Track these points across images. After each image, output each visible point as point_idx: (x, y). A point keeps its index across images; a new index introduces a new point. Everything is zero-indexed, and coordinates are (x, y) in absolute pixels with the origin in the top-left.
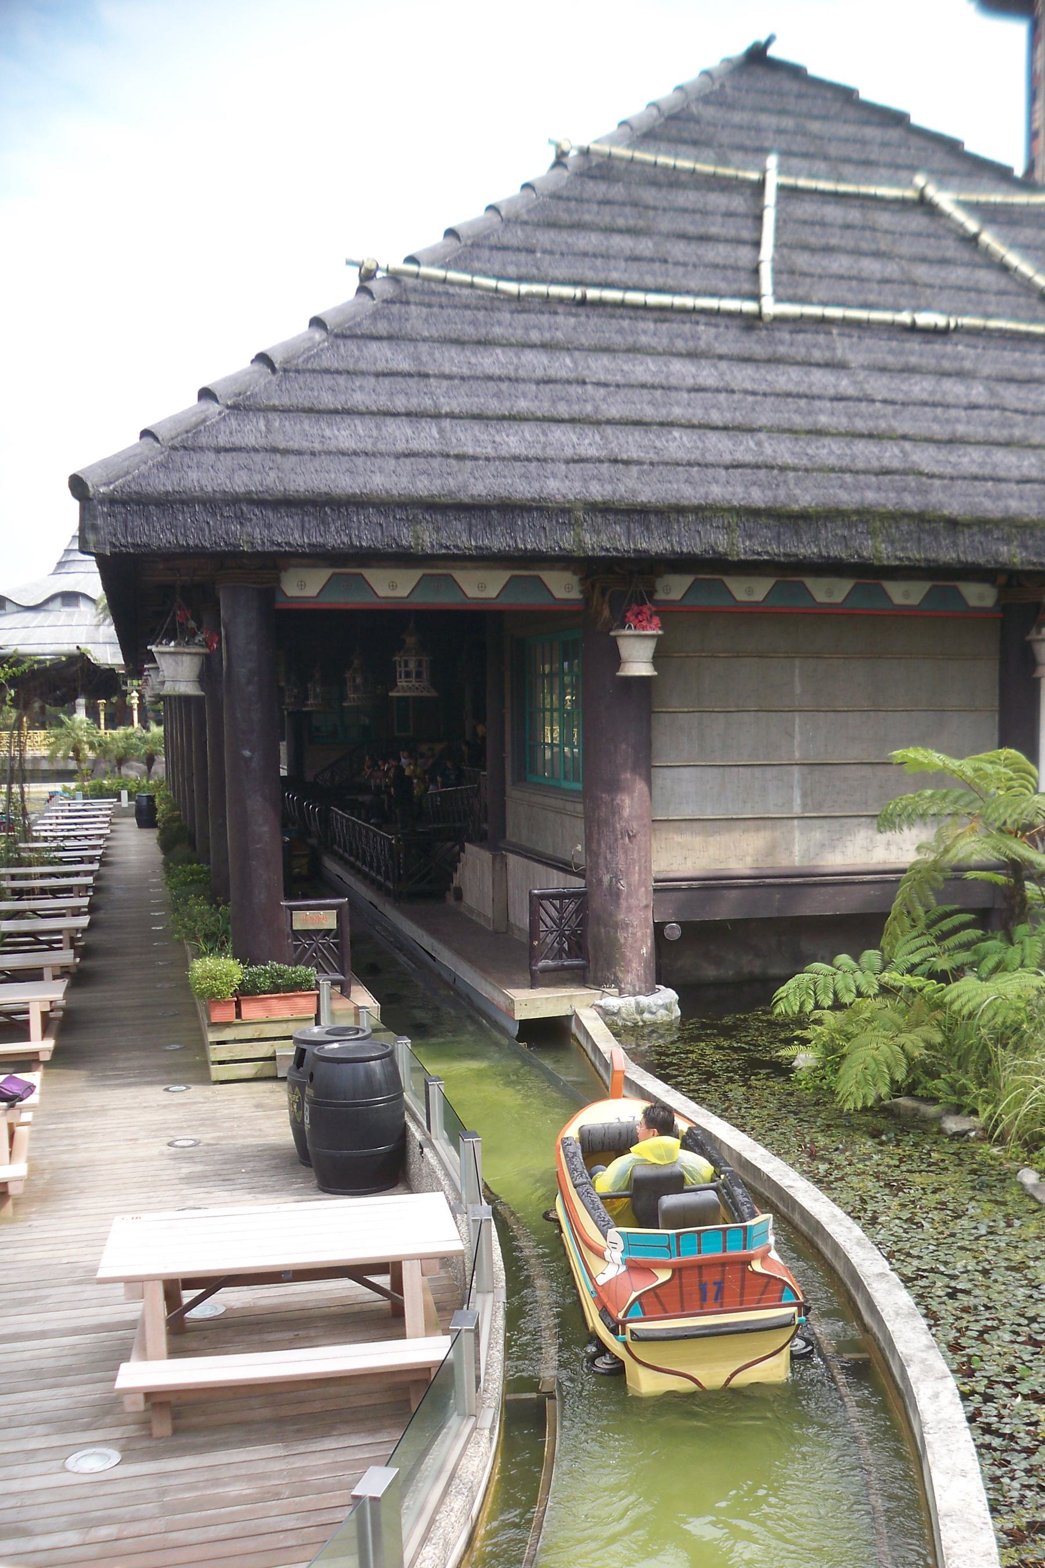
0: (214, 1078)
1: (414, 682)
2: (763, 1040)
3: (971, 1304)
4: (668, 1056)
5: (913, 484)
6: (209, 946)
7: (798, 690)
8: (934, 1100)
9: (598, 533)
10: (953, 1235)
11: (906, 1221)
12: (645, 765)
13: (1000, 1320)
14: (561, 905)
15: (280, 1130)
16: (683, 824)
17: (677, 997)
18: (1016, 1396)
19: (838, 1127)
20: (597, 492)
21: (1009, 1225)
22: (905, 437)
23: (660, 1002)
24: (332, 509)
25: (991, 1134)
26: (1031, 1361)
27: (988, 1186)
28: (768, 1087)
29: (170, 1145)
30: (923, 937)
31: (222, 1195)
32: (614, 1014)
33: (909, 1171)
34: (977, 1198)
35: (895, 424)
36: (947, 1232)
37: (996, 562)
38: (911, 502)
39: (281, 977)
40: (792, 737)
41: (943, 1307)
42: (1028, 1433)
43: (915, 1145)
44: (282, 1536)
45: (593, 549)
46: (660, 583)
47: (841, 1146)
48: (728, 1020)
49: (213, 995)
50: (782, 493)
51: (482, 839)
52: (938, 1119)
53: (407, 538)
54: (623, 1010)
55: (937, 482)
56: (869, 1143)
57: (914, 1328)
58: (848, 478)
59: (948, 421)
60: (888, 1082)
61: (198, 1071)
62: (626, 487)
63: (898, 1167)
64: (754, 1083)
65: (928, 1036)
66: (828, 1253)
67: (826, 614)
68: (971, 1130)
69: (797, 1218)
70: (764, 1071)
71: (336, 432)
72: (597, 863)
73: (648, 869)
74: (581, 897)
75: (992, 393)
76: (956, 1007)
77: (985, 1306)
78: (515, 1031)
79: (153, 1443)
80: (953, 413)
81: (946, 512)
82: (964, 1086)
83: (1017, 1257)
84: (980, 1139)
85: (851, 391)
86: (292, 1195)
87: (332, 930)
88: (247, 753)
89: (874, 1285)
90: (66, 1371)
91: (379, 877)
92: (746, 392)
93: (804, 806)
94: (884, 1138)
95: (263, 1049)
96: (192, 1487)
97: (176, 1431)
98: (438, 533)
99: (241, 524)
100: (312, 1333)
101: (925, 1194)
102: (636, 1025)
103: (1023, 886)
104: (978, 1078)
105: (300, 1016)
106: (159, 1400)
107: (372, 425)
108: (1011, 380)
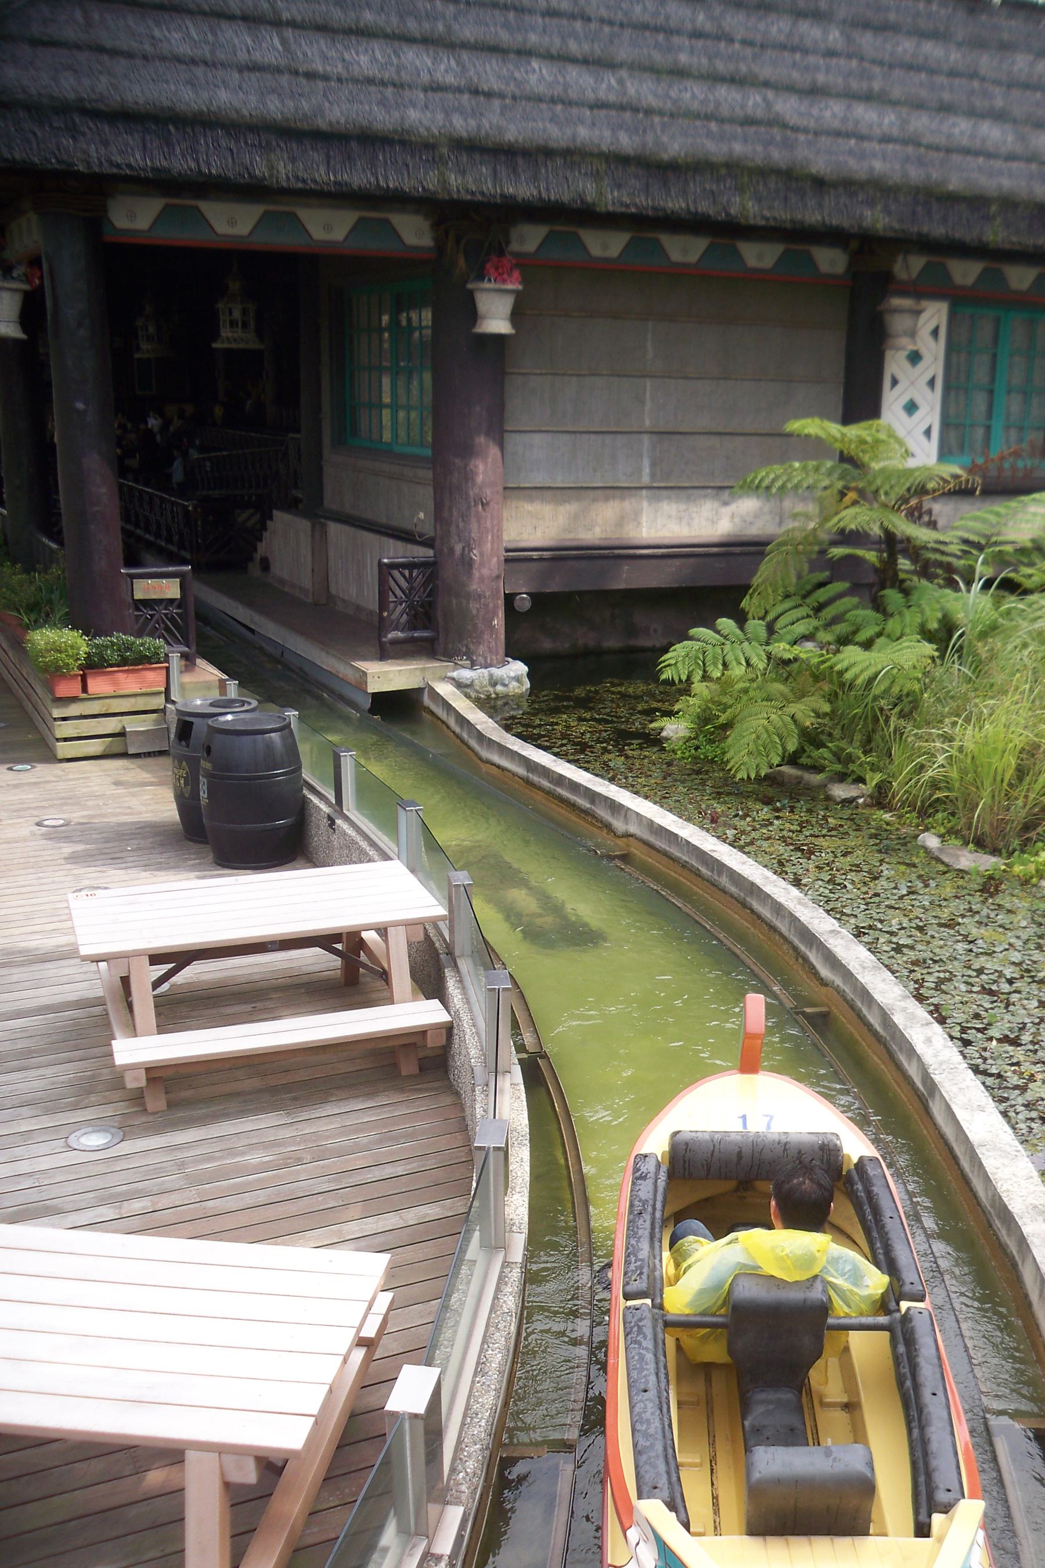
0: (60, 755)
1: (239, 333)
2: (623, 712)
3: (921, 958)
4: (534, 727)
5: (778, 138)
6: (33, 617)
7: (650, 354)
8: (817, 769)
9: (463, 173)
10: (877, 895)
11: (828, 882)
12: (498, 432)
13: (951, 973)
14: (411, 574)
15: (150, 808)
16: (534, 493)
17: (526, 669)
18: (991, 1039)
19: (729, 794)
20: (461, 126)
21: (927, 886)
22: (766, 84)
23: (512, 674)
24: (177, 128)
25: (881, 799)
26: (992, 1009)
27: (894, 850)
28: (646, 757)
29: (39, 824)
30: (801, 608)
31: (115, 874)
32: (467, 686)
33: (811, 835)
34: (887, 860)
35: (756, 69)
36: (871, 893)
37: (860, 227)
38: (778, 156)
39: (128, 649)
40: (642, 403)
41: (894, 961)
42: (1014, 1072)
43: (809, 811)
44: (320, 1198)
45: (458, 191)
46: (515, 233)
47: (740, 813)
48: (579, 692)
49: (58, 668)
50: (650, 138)
51: (292, 506)
52: (823, 786)
53: (260, 169)
54: (477, 682)
55: (802, 137)
56: (766, 810)
57: (884, 980)
58: (713, 126)
59: (807, 68)
60: (780, 752)
61: (41, 749)
62: (490, 123)
63: (800, 831)
64: (630, 753)
65: (814, 705)
66: (766, 913)
67: (679, 274)
68: (859, 797)
69: (724, 881)
70: (636, 742)
71: (167, 34)
72: (449, 532)
73: (499, 538)
74: (431, 569)
75: (849, 39)
76: (848, 676)
77: (931, 959)
78: (367, 704)
79: (150, 1118)
80: (811, 59)
81: (814, 170)
82: (850, 755)
83: (945, 915)
84: (868, 805)
85: (708, 27)
86: (191, 871)
87: (175, 600)
88: (80, 406)
89: (831, 941)
90: (27, 1054)
91: (170, 547)
92: (602, 21)
93: (653, 475)
94: (778, 804)
95: (111, 725)
96: (209, 1158)
97: (171, 1105)
98: (293, 164)
99: (74, 138)
100: (269, 1004)
101: (836, 857)
102: (489, 697)
103: (896, 560)
104: (864, 747)
105: (149, 690)
106: (165, 1078)
107: (206, 29)
108: (866, 26)
